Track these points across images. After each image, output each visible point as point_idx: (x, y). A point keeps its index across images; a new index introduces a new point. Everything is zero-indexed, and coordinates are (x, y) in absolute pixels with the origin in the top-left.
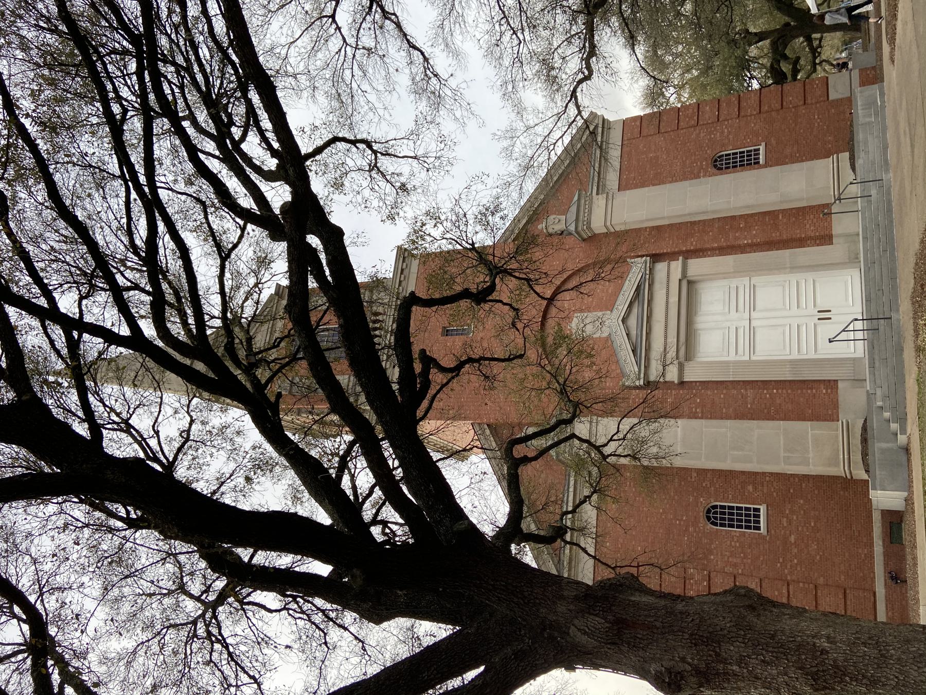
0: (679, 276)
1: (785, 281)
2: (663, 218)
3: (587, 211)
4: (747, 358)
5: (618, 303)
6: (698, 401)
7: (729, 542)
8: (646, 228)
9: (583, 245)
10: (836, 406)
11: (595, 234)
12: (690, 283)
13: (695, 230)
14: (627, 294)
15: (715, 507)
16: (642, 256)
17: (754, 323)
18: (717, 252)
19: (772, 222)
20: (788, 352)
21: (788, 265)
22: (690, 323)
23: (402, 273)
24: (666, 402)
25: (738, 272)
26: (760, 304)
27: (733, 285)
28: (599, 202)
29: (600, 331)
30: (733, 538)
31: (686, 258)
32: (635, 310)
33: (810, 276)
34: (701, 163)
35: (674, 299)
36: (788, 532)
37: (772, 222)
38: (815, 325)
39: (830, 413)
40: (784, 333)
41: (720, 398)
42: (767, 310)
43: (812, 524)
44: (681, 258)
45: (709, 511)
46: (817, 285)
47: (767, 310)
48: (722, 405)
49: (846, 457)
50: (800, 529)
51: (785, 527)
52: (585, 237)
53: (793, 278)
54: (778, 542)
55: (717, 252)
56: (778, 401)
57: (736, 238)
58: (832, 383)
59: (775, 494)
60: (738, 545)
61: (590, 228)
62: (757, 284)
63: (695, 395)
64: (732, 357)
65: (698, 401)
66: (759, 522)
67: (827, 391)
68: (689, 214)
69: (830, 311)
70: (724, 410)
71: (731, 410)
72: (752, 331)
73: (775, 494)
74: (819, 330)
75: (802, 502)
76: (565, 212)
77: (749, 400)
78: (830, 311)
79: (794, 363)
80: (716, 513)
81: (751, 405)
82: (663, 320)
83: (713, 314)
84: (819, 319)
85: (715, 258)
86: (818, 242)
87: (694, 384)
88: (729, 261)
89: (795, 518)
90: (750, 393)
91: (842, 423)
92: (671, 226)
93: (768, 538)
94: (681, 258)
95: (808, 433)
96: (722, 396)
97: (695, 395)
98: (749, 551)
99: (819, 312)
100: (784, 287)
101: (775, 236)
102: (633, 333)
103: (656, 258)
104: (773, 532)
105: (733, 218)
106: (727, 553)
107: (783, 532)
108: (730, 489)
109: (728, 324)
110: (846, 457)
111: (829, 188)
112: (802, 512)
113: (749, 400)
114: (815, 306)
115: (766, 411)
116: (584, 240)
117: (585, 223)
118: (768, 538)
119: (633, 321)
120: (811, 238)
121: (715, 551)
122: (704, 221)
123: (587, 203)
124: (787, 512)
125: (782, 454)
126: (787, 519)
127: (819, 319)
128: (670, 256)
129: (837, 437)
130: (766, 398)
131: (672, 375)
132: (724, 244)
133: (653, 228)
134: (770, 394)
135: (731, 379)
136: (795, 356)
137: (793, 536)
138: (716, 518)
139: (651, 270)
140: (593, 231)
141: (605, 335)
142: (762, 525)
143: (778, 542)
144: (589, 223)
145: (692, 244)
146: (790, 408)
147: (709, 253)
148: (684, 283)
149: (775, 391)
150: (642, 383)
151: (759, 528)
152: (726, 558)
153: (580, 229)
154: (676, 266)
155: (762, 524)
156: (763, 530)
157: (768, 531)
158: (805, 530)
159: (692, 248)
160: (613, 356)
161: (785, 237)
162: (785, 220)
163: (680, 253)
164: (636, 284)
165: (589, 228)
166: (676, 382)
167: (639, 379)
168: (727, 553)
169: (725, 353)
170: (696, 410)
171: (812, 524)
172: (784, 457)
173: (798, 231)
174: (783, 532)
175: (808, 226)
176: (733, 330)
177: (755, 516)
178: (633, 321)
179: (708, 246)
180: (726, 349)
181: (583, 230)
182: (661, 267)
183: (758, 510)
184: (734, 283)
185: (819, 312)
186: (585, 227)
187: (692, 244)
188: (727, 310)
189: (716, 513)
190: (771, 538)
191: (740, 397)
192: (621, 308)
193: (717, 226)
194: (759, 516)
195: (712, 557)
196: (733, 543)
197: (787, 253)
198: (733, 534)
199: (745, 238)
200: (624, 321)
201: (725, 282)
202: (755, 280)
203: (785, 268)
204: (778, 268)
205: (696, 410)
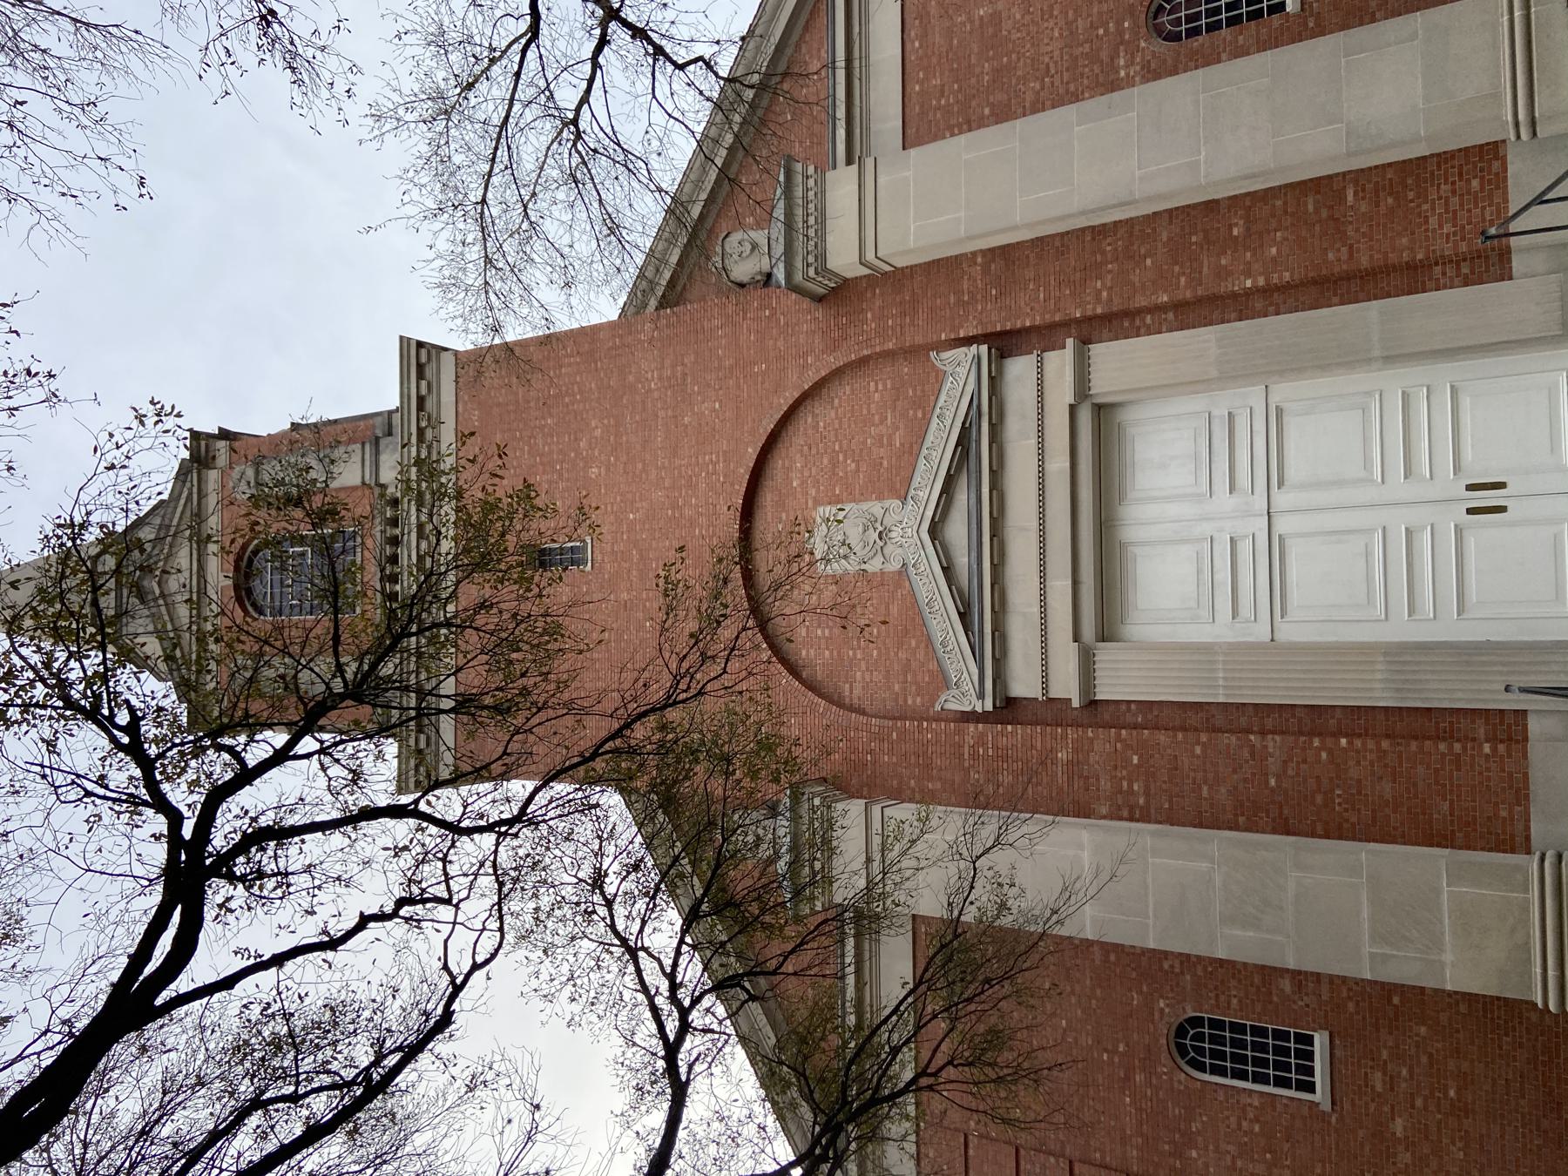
0: (1070, 399)
1: (1369, 394)
2: (1015, 228)
3: (812, 220)
4: (1261, 632)
5: (917, 479)
6: (1135, 759)
7: (1233, 1120)
8: (974, 254)
9: (819, 314)
10: (1520, 793)
11: (846, 280)
12: (1103, 412)
13: (1103, 253)
14: (936, 455)
15: (1196, 1022)
16: (968, 341)
17: (1282, 525)
18: (1171, 315)
19: (1324, 213)
20: (1379, 611)
21: (1376, 353)
22: (1105, 526)
23: (421, 407)
24: (1054, 762)
25: (1230, 375)
26: (1292, 473)
27: (1221, 412)
28: (842, 186)
29: (879, 558)
30: (1244, 1110)
31: (1085, 341)
32: (962, 498)
33: (1445, 373)
34: (1119, 23)
35: (1058, 464)
36: (1386, 1109)
37: (1324, 213)
38: (1459, 530)
39: (1504, 814)
40: (1368, 554)
41: (1194, 755)
42: (1318, 485)
43: (1452, 1093)
44: (1070, 342)
45: (1181, 1032)
46: (1466, 402)
47: (1318, 485)
48: (1200, 775)
49: (1551, 973)
50: (1419, 1102)
51: (1379, 1095)
52: (821, 291)
53: (1394, 381)
54: (1361, 1133)
55: (1171, 315)
56: (1354, 773)
57: (1222, 273)
58: (1510, 720)
59: (1351, 1006)
60: (1257, 1128)
61: (826, 269)
62: (1284, 405)
63: (1054, 1014)
64: (1222, 630)
65: (1135, 759)
66: (1310, 1071)
67: (1494, 749)
68: (1083, 213)
69: (1500, 485)
70: (1205, 791)
71: (1223, 790)
72: (1277, 549)
73: (1351, 1006)
74: (1471, 543)
75: (1423, 1030)
76: (765, 221)
77: (1273, 764)
78: (1500, 485)
79: (1401, 655)
80: (1199, 1037)
81: (1278, 777)
82: (1034, 524)
83: (1168, 499)
84: (1470, 511)
85: (1166, 337)
86: (1465, 270)
87: (1124, 707)
88: (1205, 340)
89: (1404, 1072)
90: (1274, 743)
91: (1542, 859)
92: (1040, 243)
93: (1333, 1120)
94: (1070, 342)
95: (1437, 892)
96: (1198, 750)
97: (1054, 1014)
98: (1286, 1146)
99: (1471, 488)
100: (1365, 410)
101: (1336, 259)
102: (962, 560)
103: (1004, 344)
104: (1347, 1106)
105: (1211, 206)
106: (1231, 1148)
107: (1372, 1107)
108: (1233, 983)
109: (1207, 529)
110: (1551, 973)
111: (1496, 97)
112: (1424, 1059)
113: (1273, 764)
114: (1457, 469)
115: (1319, 799)
116: (820, 299)
117: (811, 259)
118: (1333, 1120)
119: (957, 531)
120: (1444, 261)
121: (1200, 1139)
122: (1130, 222)
123: (811, 182)
124: (1385, 1054)
125: (1367, 949)
126: (1385, 1074)
127: (1470, 511)
128: (1041, 337)
129: (1525, 908)
130: (1319, 761)
131: (1066, 686)
132: (1188, 294)
133: (992, 252)
134: (1330, 752)
135: (1221, 700)
136: (1402, 630)
137: (1399, 1121)
138: (1200, 1051)
139: (995, 382)
140: (837, 275)
141: (895, 566)
142: (1318, 1079)
143: (1361, 1133)
144: (822, 257)
145: (1098, 299)
146: (1388, 796)
147: (1148, 319)
148: (1085, 417)
149: (1344, 741)
150: (989, 707)
151: (1310, 1088)
152: (1229, 1158)
153: (798, 277)
154: (1061, 362)
155: (1320, 1077)
156: (1321, 1095)
157: (1333, 1103)
158: (1432, 1108)
159: (1099, 311)
160: (915, 620)
161: (1364, 262)
162: (1364, 207)
163: (1066, 325)
164: (958, 424)
165: (823, 270)
166: (1076, 703)
167: (981, 696)
168: (1231, 1148)
169: (1205, 613)
170: (1130, 786)
171: (1452, 1093)
172: (1372, 956)
173: (1404, 241)
174: (1372, 1107)
175: (1433, 222)
176: (1223, 550)
177: (1301, 1054)
178: (957, 531)
179: (1140, 301)
180: (1206, 599)
181: (808, 279)
182: (1020, 369)
183: (1309, 1040)
184: (1221, 402)
185: (1471, 488)
186: (812, 272)
187: (1098, 299)
188: (1205, 487)
189: (1199, 1037)
190: (1341, 1119)
191: (1246, 755)
192: (923, 495)
193: (1165, 237)
194: (1310, 1056)
195: (1194, 1154)
196: (1245, 1124)
197: (1372, 311)
198: (1245, 1100)
199: (1248, 274)
200: (935, 531)
201: (1195, 404)
202: (1283, 392)
203: (1369, 361)
204: (1351, 358)
205: (1130, 786)
